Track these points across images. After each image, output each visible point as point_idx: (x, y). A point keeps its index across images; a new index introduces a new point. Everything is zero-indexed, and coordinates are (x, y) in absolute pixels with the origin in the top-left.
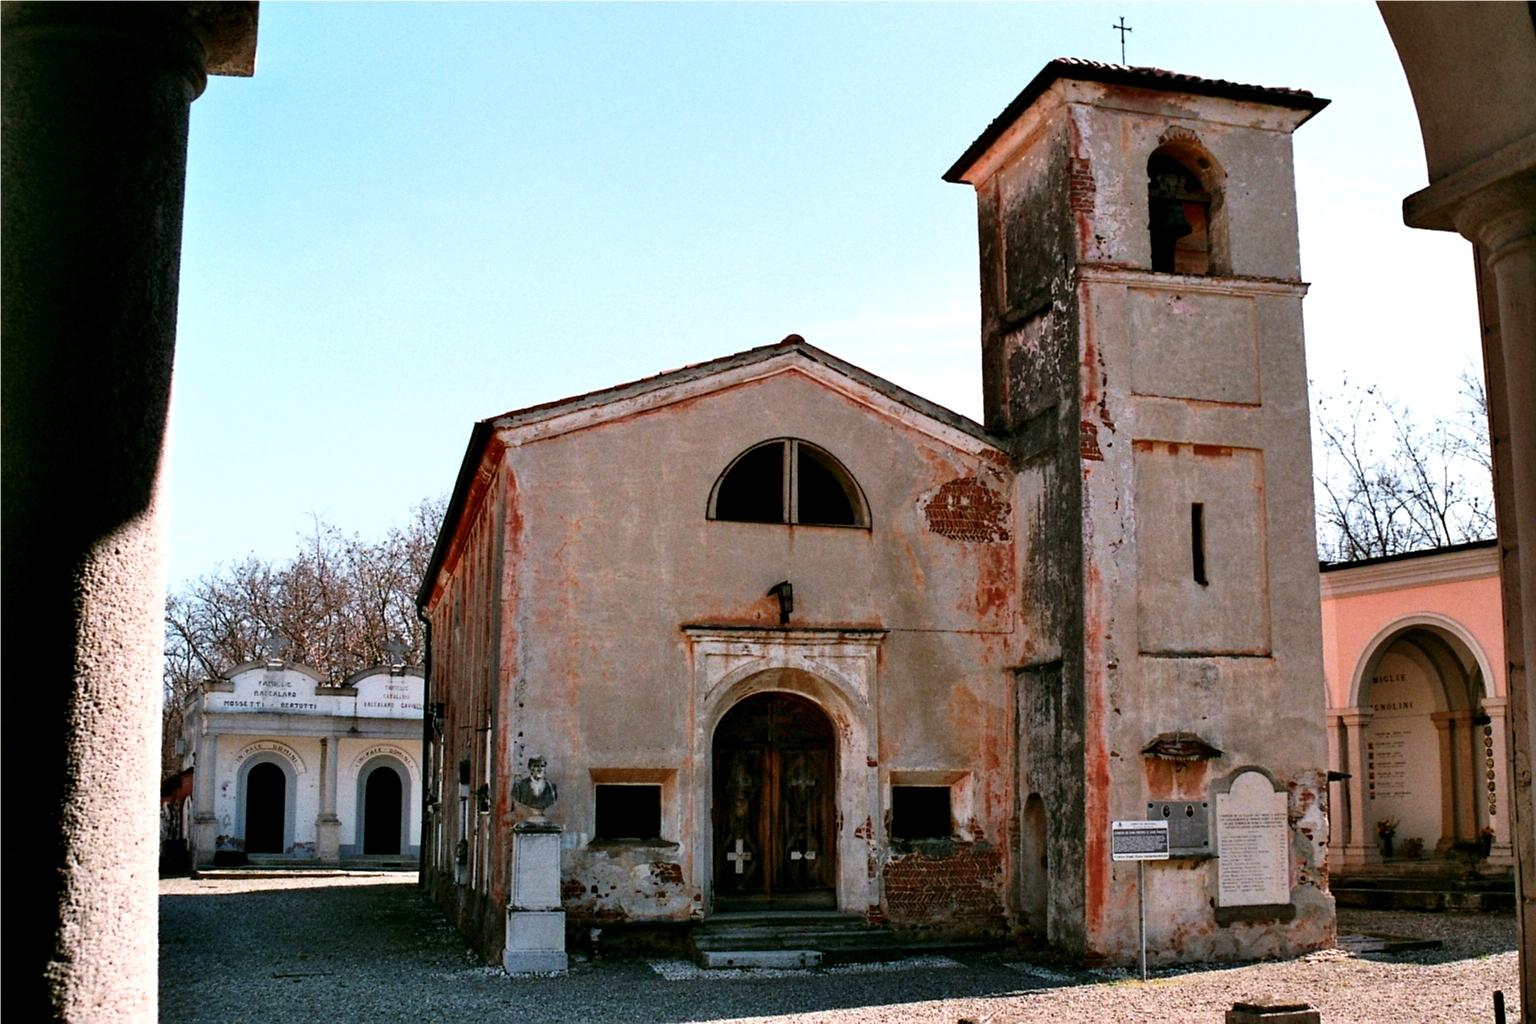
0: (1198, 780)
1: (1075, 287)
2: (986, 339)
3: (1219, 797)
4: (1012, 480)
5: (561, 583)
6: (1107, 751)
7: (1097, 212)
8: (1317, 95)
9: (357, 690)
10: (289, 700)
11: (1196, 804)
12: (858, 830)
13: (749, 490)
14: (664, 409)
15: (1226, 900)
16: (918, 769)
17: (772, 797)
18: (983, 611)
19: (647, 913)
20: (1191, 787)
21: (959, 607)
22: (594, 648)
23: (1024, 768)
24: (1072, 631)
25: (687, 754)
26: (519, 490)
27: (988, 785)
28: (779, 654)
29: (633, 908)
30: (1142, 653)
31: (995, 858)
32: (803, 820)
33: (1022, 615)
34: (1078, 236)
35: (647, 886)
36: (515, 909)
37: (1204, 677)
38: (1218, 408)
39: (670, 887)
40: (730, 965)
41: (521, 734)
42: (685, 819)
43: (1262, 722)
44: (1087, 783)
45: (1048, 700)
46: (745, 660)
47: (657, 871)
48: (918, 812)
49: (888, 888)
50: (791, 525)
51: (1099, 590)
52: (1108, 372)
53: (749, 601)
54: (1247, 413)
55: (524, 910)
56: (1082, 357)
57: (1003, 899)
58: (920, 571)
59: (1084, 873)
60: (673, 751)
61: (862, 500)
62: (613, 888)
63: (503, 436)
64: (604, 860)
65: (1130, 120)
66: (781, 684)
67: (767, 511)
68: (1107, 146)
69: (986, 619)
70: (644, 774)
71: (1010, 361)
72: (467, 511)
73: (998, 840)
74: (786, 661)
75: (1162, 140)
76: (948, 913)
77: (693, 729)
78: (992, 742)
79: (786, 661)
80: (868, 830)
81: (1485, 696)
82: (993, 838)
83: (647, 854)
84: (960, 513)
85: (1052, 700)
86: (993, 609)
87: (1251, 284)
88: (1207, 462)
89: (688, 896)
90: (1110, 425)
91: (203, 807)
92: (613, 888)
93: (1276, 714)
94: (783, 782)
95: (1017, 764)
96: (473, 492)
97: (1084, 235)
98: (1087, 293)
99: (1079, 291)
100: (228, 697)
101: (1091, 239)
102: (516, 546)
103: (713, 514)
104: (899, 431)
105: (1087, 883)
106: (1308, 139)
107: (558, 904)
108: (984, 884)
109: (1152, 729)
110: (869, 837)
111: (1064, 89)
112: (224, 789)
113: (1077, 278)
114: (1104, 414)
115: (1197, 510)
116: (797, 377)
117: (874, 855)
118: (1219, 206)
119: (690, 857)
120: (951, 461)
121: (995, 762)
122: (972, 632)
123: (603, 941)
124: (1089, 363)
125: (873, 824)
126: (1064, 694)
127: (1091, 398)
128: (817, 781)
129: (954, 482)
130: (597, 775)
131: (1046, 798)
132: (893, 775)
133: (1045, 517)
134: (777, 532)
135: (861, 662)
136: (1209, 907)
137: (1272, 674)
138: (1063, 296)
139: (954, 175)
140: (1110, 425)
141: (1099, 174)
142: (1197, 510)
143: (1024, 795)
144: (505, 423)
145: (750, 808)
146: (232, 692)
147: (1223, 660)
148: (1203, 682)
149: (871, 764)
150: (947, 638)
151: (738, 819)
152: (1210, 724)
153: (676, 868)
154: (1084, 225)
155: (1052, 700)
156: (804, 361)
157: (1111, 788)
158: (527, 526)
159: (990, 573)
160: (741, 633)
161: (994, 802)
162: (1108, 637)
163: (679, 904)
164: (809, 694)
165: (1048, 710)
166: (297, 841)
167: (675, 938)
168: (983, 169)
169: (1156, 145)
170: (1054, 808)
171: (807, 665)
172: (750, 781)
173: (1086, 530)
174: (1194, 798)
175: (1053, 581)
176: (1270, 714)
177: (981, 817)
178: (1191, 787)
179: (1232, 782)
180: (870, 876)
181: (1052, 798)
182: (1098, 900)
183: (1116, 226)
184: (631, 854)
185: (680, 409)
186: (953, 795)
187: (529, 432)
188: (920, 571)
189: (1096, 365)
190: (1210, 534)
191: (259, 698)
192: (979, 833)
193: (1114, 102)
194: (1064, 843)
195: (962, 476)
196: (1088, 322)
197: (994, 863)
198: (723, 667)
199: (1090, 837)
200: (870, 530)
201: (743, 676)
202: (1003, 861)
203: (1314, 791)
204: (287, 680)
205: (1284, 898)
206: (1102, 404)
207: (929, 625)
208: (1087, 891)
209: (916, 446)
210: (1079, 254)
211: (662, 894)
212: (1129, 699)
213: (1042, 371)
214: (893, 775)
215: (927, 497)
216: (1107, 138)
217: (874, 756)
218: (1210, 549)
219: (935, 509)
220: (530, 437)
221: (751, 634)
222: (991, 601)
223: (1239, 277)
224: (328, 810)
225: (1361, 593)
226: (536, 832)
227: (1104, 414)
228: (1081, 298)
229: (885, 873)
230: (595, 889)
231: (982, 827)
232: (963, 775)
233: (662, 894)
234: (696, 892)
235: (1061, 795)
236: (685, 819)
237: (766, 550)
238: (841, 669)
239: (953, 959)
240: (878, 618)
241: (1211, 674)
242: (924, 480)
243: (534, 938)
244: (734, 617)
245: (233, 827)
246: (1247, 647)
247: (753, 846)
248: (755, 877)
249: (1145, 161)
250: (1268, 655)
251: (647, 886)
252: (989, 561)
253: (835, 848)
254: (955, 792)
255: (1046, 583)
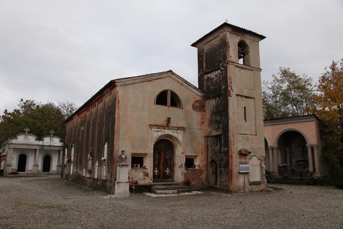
0: (246, 159)
1: (227, 65)
2: (200, 75)
3: (250, 161)
4: (206, 101)
5: (127, 115)
6: (233, 152)
7: (230, 52)
8: (264, 35)
9: (43, 140)
10: (29, 141)
11: (246, 162)
12: (179, 166)
13: (162, 99)
14: (147, 82)
15: (251, 180)
16: (190, 155)
17: (162, 160)
18: (201, 125)
19: (142, 183)
20: (245, 159)
21: (197, 124)
22: (133, 128)
23: (210, 155)
24: (226, 129)
25: (150, 150)
26: (119, 95)
27: (201, 158)
28: (167, 132)
29: (139, 182)
30: (238, 134)
31: (202, 172)
32: (168, 164)
33: (208, 126)
34: (227, 56)
35: (142, 177)
36: (244, 176)
37: (247, 139)
38: (248, 90)
39: (146, 177)
40: (161, 193)
41: (118, 145)
42: (149, 163)
43: (256, 147)
44: (229, 158)
45: (217, 142)
46: (160, 133)
47: (144, 174)
48: (189, 162)
49: (185, 178)
50: (169, 106)
51: (231, 121)
52: (232, 81)
53: (162, 121)
54: (253, 91)
55: (121, 182)
56: (228, 78)
57: (204, 180)
58: (191, 117)
59: (229, 174)
60: (147, 150)
61: (182, 104)
62: (136, 178)
63: (117, 84)
64: (134, 172)
65: (235, 36)
66: (166, 137)
67: (165, 104)
68: (232, 40)
69: (201, 127)
70: (141, 154)
71: (206, 79)
72: (93, 101)
73: (203, 168)
74: (168, 133)
75: (240, 40)
76: (195, 182)
77: (151, 145)
78: (89, 160)
79: (168, 133)
80: (182, 166)
81: (307, 144)
82: (202, 168)
83: (142, 171)
84: (197, 107)
85: (219, 142)
86: (202, 125)
87: (253, 68)
88: (246, 99)
89: (150, 179)
90: (232, 91)
91: (8, 163)
92: (136, 178)
93: (257, 146)
94: (164, 157)
95: (208, 154)
96: (99, 97)
97: (228, 55)
98: (229, 66)
99: (228, 66)
100: (16, 140)
101: (229, 56)
102: (118, 106)
103: (155, 103)
104: (187, 90)
105: (230, 176)
106: (262, 43)
107: (128, 181)
108: (201, 177)
109: (239, 148)
110: (182, 167)
111: (226, 29)
112: (13, 159)
113: (227, 63)
114: (232, 89)
115: (245, 108)
116: (171, 78)
117: (183, 171)
118: (247, 54)
119: (150, 171)
120: (196, 97)
121: (202, 154)
122: (199, 129)
123: (137, 189)
124: (229, 79)
125: (183, 165)
126: (222, 141)
127: (230, 86)
128: (170, 157)
129: (196, 101)
130: (132, 154)
131: (217, 161)
132: (186, 156)
133: (215, 108)
134: (166, 108)
135: (181, 134)
136: (248, 182)
137: (257, 138)
138: (223, 67)
139: (194, 45)
140: (232, 91)
141: (230, 44)
142: (245, 108)
143: (210, 160)
144: (117, 81)
145: (158, 162)
146: (17, 139)
147: (250, 136)
148: (247, 139)
149: (183, 153)
150: (195, 130)
151: (156, 164)
152: (248, 148)
153: (147, 173)
154: (228, 54)
155: (219, 142)
156: (172, 75)
157: (233, 158)
158: (121, 102)
159: (202, 118)
160: (161, 127)
161: (202, 161)
162: (233, 130)
163: (148, 181)
164: (170, 139)
165: (217, 144)
166: (29, 169)
167: (148, 188)
168: (200, 45)
169: (239, 41)
170: (219, 162)
171: (172, 134)
172: (158, 156)
173: (229, 110)
174: (246, 161)
175: (218, 120)
176: (257, 146)
177: (200, 164)
178: (245, 159)
179: (251, 158)
180: (182, 175)
181: (219, 161)
182: (231, 180)
183: (233, 55)
184: (139, 171)
185: (150, 82)
186: (194, 160)
187: (122, 83)
188: (191, 117)
189: (230, 79)
190: (247, 113)
191: (23, 141)
192: (200, 167)
193: (233, 32)
194: (223, 169)
195: (198, 100)
196: (229, 72)
197: (202, 173)
198: (156, 134)
199: (230, 168)
200: (182, 109)
201: (160, 135)
202: (204, 173)
203: (263, 160)
204: (29, 137)
205: (259, 180)
206: (231, 87)
207: (192, 127)
208: (230, 178)
209: (190, 93)
210: (227, 59)
211: (145, 179)
212: (236, 142)
213: (215, 81)
214: (186, 156)
215: (192, 103)
216: (232, 38)
217: (183, 152)
218: (247, 116)
219: (193, 105)
220: (122, 85)
221: (162, 127)
222: (202, 124)
223: (251, 67)
224: (36, 163)
225: (291, 123)
226: (124, 166)
227: (232, 89)
228: (228, 67)
229: (184, 175)
230: (132, 178)
231: (200, 166)
232: (197, 156)
233: (145, 179)
234: (151, 178)
235: (222, 160)
236: (149, 163)
237: (165, 111)
238: (177, 135)
239: (201, 192)
240: (184, 125)
241: (248, 138)
242: (191, 100)
243: (122, 189)
244: (159, 123)
245: (15, 167)
246: (252, 134)
247: (159, 169)
248: (159, 176)
249: (237, 43)
250: (256, 135)
251: (142, 177)
252: (202, 116)
253: (173, 170)
254: (195, 160)
255: (216, 120)
